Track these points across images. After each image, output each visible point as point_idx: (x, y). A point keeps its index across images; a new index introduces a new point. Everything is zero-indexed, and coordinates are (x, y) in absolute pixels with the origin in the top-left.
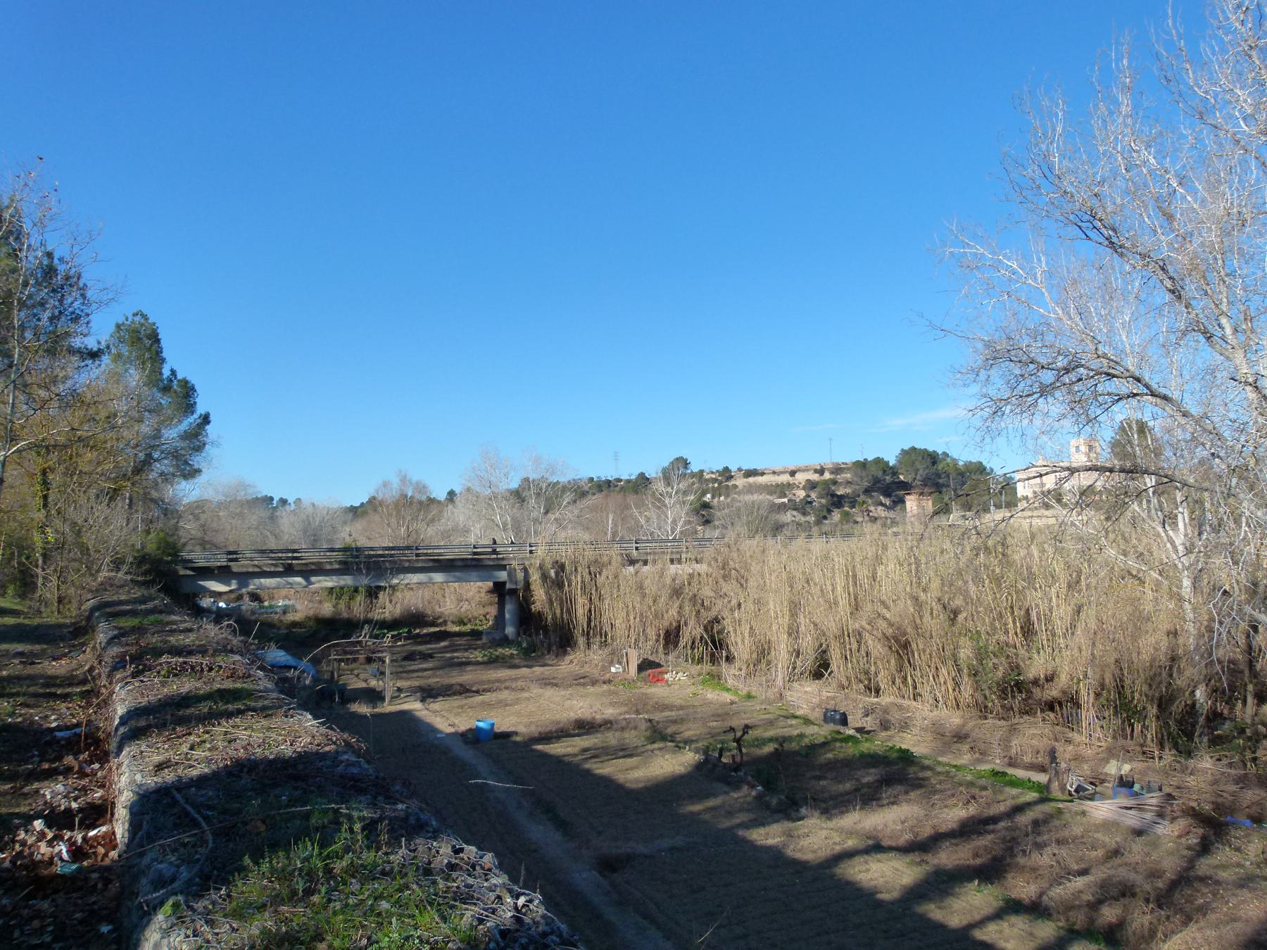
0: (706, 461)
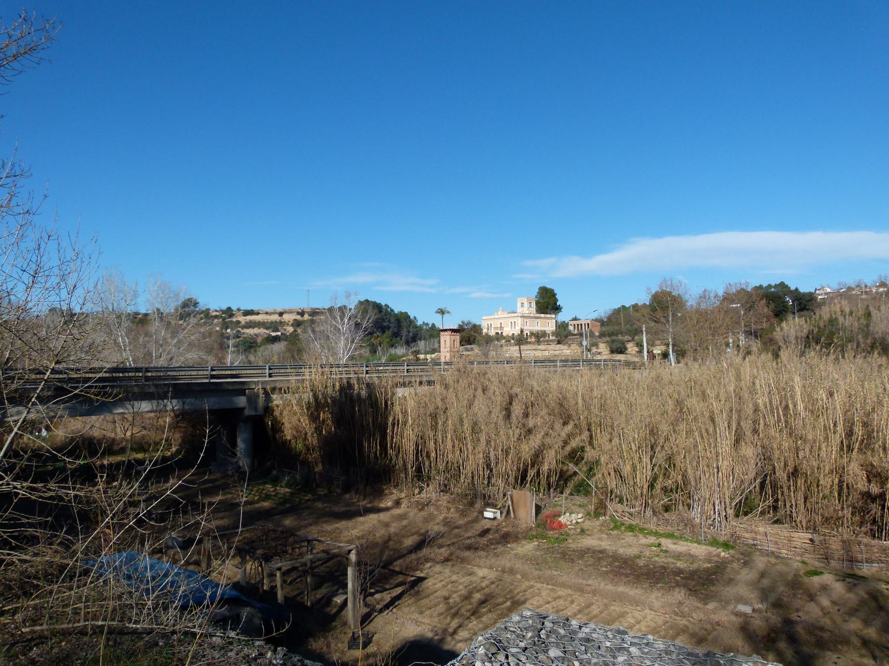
0: (213, 300)
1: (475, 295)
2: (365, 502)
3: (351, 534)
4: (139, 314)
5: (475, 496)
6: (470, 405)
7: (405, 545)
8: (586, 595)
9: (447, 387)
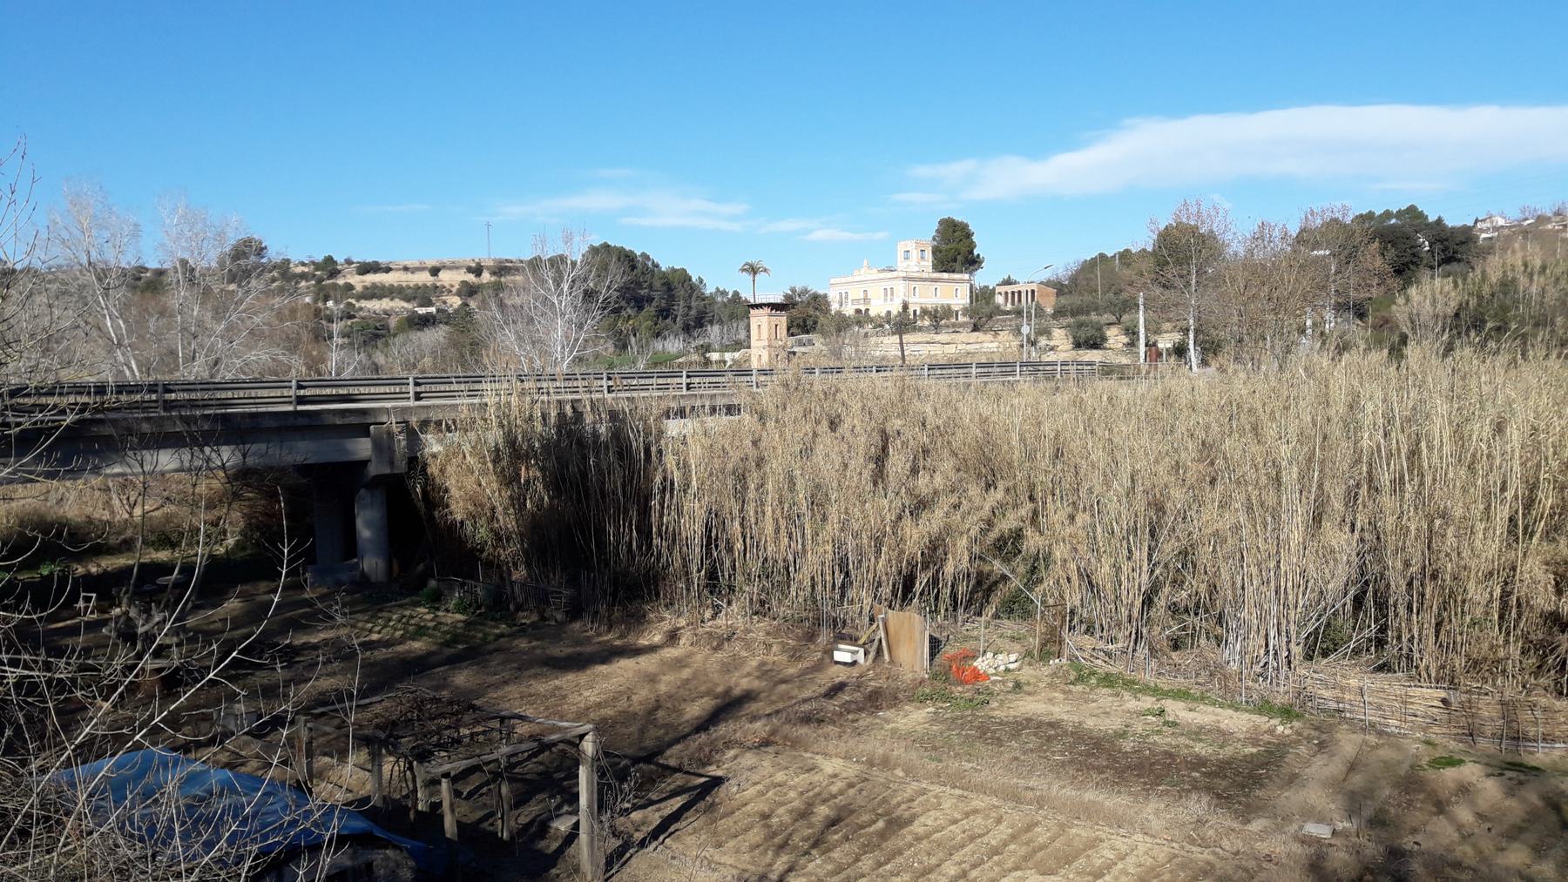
0: (296, 244)
1: (819, 235)
2: (610, 636)
3: (585, 699)
4: (147, 270)
5: (818, 622)
6: (807, 452)
7: (687, 717)
8: (1023, 807)
9: (762, 417)
